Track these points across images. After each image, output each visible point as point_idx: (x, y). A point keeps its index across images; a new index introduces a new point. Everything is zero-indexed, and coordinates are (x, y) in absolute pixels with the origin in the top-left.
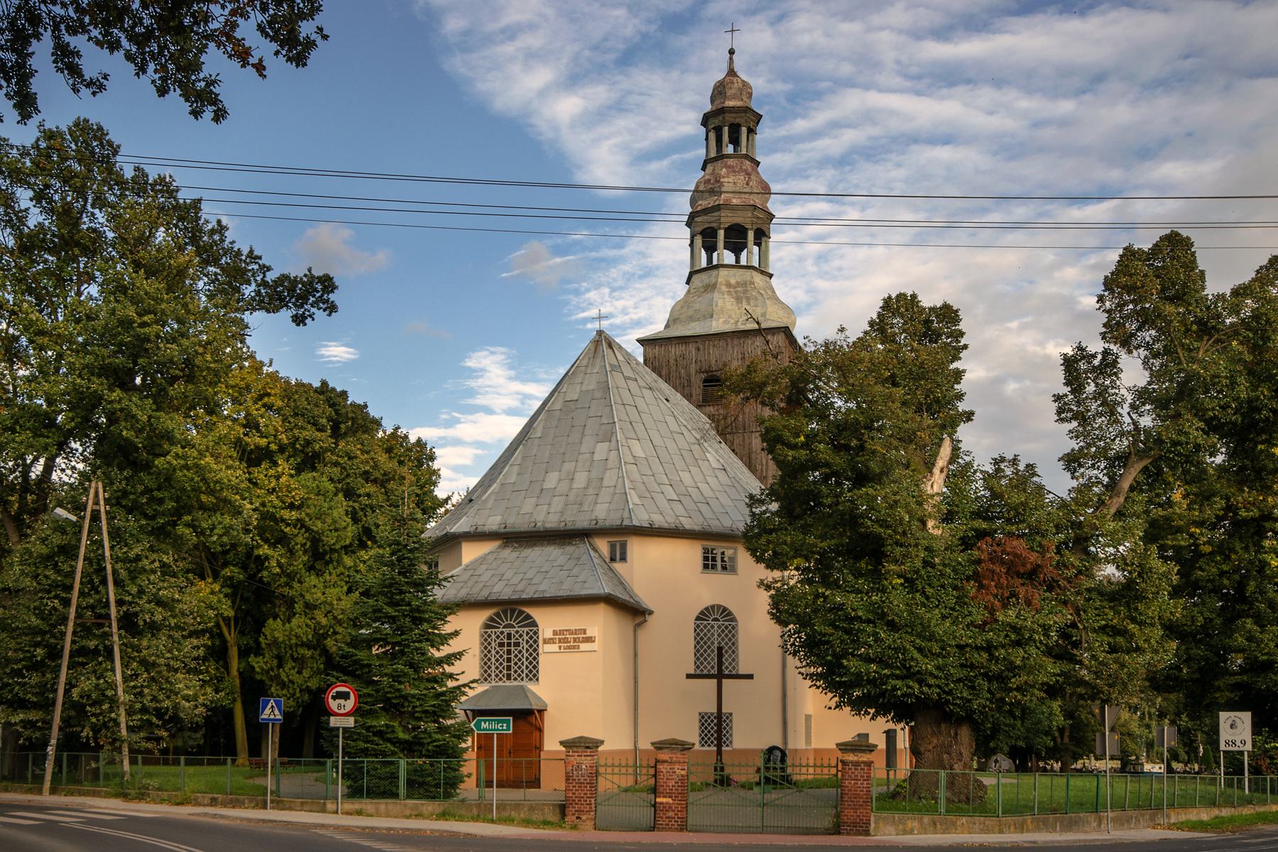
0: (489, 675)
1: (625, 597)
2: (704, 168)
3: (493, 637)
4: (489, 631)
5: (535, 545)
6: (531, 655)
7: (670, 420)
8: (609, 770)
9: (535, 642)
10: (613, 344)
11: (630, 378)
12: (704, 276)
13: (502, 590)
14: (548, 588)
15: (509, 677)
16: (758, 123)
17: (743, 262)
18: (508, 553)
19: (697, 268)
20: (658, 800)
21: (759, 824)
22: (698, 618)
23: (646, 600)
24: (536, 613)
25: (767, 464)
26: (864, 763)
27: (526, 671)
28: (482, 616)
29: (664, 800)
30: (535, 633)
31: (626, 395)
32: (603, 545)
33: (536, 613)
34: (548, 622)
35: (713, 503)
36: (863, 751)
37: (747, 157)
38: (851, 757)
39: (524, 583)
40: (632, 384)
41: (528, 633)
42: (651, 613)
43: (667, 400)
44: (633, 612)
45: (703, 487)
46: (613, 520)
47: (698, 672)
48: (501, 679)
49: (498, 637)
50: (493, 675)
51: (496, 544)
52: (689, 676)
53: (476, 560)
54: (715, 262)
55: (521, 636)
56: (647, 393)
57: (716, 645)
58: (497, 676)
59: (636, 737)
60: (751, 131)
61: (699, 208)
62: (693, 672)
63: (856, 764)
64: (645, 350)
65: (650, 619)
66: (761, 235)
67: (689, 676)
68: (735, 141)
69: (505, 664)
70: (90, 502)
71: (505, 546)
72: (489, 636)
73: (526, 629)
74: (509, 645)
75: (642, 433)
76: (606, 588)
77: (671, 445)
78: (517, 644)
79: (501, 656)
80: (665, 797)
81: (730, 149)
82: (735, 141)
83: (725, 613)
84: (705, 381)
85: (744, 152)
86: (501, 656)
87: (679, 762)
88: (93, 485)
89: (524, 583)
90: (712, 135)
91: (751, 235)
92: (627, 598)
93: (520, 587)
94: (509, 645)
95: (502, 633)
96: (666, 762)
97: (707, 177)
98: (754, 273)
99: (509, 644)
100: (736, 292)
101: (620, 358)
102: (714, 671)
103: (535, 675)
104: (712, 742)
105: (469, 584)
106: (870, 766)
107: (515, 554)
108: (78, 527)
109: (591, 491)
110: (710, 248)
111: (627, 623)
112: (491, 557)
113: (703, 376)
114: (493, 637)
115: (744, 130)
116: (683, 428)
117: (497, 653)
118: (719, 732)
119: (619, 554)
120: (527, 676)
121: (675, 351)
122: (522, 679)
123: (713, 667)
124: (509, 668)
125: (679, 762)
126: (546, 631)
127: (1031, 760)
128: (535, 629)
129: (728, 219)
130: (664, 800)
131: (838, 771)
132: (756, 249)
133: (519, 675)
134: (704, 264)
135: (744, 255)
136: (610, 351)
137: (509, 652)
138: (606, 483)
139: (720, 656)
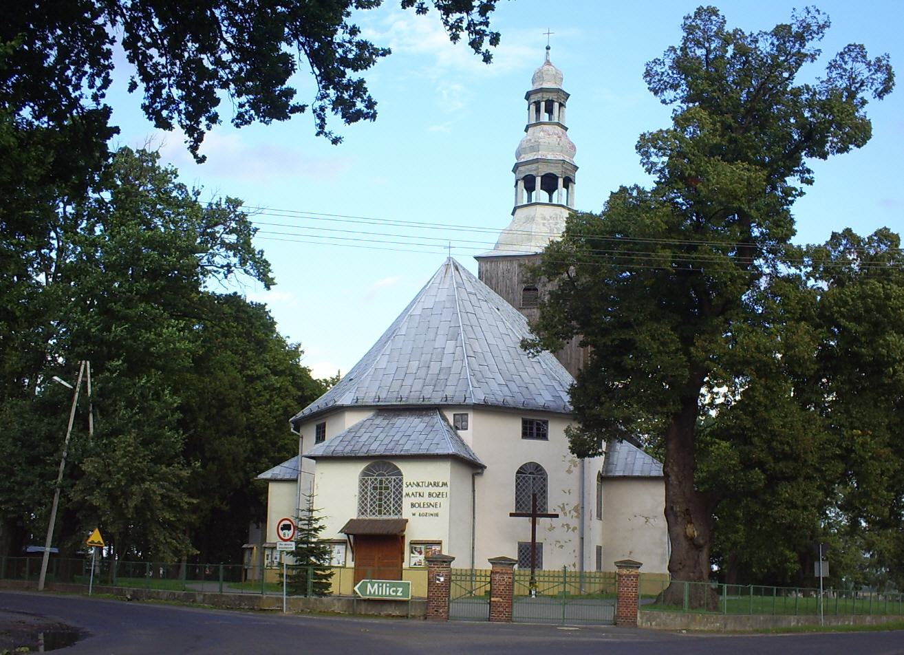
0: (366, 511)
1: (467, 456)
2: (526, 130)
3: (369, 482)
4: (366, 478)
5: (398, 416)
6: (397, 496)
7: (500, 324)
8: (459, 578)
9: (400, 487)
10: (459, 267)
11: (471, 293)
12: (525, 210)
13: (377, 448)
14: (410, 447)
15: (380, 513)
16: (566, 100)
17: (555, 201)
18: (378, 421)
19: (519, 205)
20: (492, 599)
21: (562, 617)
22: (518, 472)
23: (482, 460)
24: (403, 467)
25: (571, 354)
26: (634, 576)
27: (392, 508)
28: (360, 467)
29: (496, 599)
30: (401, 480)
31: (467, 304)
32: (450, 416)
33: (403, 467)
34: (410, 472)
35: (531, 387)
36: (632, 567)
37: (558, 124)
38: (625, 572)
39: (393, 443)
40: (472, 297)
41: (395, 481)
42: (486, 467)
43: (498, 309)
44: (474, 467)
45: (524, 375)
46: (458, 399)
47: (518, 512)
48: (374, 514)
49: (373, 483)
50: (368, 511)
51: (369, 414)
52: (512, 515)
53: (356, 425)
54: (533, 201)
55: (390, 482)
56: (483, 304)
57: (531, 492)
58: (371, 511)
59: (473, 563)
60: (561, 105)
61: (522, 160)
62: (514, 512)
63: (628, 576)
64: (480, 265)
65: (485, 471)
66: (568, 182)
67: (512, 515)
68: (549, 110)
69: (377, 503)
70: (81, 375)
71: (377, 415)
72: (366, 482)
73: (393, 477)
74: (381, 488)
75: (480, 335)
76: (451, 450)
77: (501, 345)
78: (387, 488)
79: (375, 497)
80: (497, 597)
81: (545, 117)
82: (549, 110)
83: (491, 44)
84: (525, 290)
85: (556, 121)
86: (375, 497)
87: (507, 573)
88: (83, 362)
89: (393, 443)
90: (533, 108)
91: (561, 182)
92: (468, 456)
93: (390, 446)
94: (381, 488)
95: (376, 479)
96: (498, 572)
97: (529, 138)
98: (563, 210)
99: (380, 489)
100: (549, 224)
101: (464, 278)
102: (530, 511)
103: (399, 512)
104: (528, 565)
105: (353, 443)
106: (637, 578)
107: (386, 422)
108: (72, 392)
109: (442, 377)
110: (530, 188)
111: (466, 473)
112: (368, 423)
113: (524, 286)
114: (369, 482)
115: (556, 105)
116: (509, 330)
117: (372, 494)
118: (533, 556)
119: (460, 424)
120: (394, 512)
121: (502, 266)
122: (390, 514)
123: (529, 509)
124: (380, 506)
125: (507, 573)
126: (407, 479)
127: (65, 217)
128: (400, 477)
129: (545, 170)
130: (496, 599)
131: (616, 581)
132: (565, 190)
133: (388, 511)
134: (525, 202)
135: (555, 194)
136: (457, 272)
137: (381, 494)
138: (453, 371)
139: (535, 500)
